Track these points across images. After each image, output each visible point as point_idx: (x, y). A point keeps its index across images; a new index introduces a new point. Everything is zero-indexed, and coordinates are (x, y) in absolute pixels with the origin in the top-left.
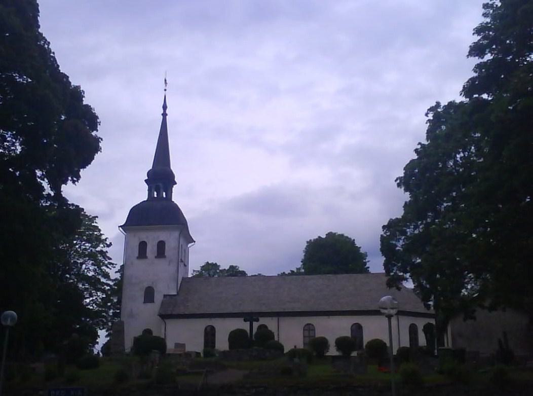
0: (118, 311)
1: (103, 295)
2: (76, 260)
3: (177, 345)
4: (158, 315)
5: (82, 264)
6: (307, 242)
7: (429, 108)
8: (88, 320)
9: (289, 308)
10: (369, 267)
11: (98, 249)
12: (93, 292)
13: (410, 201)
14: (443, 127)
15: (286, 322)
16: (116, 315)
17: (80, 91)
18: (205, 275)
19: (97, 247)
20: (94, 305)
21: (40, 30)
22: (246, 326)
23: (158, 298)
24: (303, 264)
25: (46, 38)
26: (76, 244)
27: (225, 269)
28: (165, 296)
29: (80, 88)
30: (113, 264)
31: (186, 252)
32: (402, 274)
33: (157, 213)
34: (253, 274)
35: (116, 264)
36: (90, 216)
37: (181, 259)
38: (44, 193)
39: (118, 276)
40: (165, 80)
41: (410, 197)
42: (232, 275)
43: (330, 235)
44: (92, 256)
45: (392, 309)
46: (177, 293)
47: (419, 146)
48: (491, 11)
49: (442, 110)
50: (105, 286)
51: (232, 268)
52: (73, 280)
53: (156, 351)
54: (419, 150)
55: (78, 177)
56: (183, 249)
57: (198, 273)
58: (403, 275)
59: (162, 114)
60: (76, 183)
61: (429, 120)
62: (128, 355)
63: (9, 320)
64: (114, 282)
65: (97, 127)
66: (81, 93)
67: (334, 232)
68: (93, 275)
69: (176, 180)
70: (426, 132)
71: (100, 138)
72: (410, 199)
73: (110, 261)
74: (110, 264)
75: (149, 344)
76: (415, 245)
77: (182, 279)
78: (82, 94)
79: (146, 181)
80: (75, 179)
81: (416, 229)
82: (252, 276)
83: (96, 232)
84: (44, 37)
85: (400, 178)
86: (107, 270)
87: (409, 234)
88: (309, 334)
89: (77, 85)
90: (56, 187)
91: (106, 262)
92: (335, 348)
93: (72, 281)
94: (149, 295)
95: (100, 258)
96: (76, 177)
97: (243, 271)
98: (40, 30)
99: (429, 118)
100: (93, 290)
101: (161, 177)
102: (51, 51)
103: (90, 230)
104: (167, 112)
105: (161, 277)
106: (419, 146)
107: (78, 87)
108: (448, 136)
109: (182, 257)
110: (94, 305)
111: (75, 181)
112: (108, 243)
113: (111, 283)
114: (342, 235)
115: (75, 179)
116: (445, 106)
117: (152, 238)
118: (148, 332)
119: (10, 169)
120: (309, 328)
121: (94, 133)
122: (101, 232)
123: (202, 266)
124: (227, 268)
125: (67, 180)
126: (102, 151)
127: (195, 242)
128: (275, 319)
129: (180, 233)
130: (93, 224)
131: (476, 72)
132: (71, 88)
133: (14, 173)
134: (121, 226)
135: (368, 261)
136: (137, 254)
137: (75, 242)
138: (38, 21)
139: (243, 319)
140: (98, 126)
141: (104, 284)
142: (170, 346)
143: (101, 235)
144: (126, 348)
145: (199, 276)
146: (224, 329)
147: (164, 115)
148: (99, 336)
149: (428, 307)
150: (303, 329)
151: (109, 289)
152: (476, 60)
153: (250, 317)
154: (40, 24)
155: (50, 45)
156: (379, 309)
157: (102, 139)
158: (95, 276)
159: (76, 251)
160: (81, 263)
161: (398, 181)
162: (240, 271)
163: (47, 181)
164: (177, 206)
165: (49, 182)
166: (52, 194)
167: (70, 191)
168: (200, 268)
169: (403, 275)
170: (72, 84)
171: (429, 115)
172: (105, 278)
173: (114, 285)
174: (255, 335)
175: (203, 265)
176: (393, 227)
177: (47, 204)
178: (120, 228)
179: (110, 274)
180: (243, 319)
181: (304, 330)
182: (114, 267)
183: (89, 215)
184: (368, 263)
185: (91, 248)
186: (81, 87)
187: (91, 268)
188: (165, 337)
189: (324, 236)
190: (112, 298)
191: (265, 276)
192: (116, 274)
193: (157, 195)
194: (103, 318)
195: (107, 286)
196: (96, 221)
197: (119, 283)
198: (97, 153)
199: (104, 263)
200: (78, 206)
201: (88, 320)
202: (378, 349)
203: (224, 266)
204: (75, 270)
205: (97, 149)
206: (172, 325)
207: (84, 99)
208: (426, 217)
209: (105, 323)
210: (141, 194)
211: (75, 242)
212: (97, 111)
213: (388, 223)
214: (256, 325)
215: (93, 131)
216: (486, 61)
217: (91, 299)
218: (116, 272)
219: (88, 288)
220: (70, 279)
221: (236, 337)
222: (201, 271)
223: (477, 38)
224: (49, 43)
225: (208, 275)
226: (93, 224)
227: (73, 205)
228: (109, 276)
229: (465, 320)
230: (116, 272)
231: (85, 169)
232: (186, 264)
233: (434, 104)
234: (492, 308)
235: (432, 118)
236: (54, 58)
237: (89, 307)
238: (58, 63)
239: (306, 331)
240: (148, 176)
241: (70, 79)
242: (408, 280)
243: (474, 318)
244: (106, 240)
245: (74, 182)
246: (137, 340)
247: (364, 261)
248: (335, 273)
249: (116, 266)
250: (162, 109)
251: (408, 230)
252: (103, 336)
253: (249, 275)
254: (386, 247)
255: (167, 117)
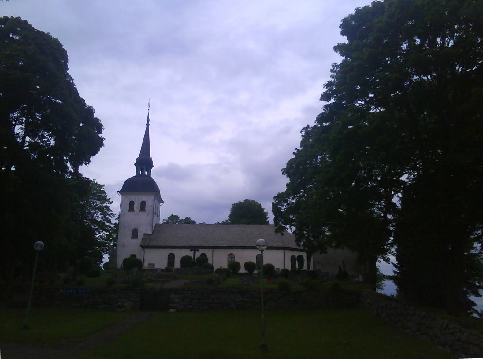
0: (116, 243)
1: (106, 233)
2: (90, 211)
3: (150, 264)
4: (140, 246)
5: (94, 213)
6: (233, 205)
7: (303, 128)
8: (97, 248)
9: (220, 243)
10: (268, 221)
11: (104, 205)
12: (100, 231)
13: (290, 183)
14: (311, 140)
15: (218, 252)
16: (115, 245)
17: (92, 109)
18: (170, 222)
19: (104, 203)
20: (101, 239)
21: (68, 72)
22: (191, 254)
23: (140, 235)
24: (230, 218)
25: (71, 76)
26: (91, 201)
27: (183, 219)
28: (145, 234)
29: (92, 107)
30: (113, 214)
31: (158, 208)
32: (284, 225)
33: (142, 184)
34: (200, 223)
35: (115, 214)
36: (100, 184)
37: (155, 213)
38: (68, 170)
39: (117, 221)
40: (149, 104)
41: (290, 181)
42: (186, 223)
43: (246, 201)
44: (101, 209)
45: (263, 246)
46: (152, 233)
47: (296, 151)
48: (335, 74)
49: (310, 130)
50: (108, 228)
51: (187, 218)
52: (88, 223)
53: (136, 267)
54: (296, 153)
55: (89, 161)
56: (157, 206)
57: (166, 221)
58: (285, 226)
59: (146, 124)
60: (88, 165)
61: (302, 136)
62: (119, 269)
63: (39, 246)
64: (114, 225)
65: (102, 131)
66: (93, 110)
67: (249, 199)
68: (101, 221)
69: (153, 164)
70: (300, 142)
71: (103, 138)
72: (290, 182)
73: (112, 212)
74: (112, 214)
75: (133, 263)
76: (292, 209)
77: (155, 225)
78: (94, 111)
79: (135, 164)
80: (87, 162)
81: (293, 199)
82: (199, 224)
83: (103, 194)
84: (70, 76)
85: (284, 169)
86: (110, 218)
87: (289, 202)
88: (231, 260)
89: (91, 105)
90: (76, 168)
91: (109, 213)
92: (244, 268)
93: (87, 224)
94: (135, 234)
95: (105, 210)
96: (88, 161)
97: (194, 221)
98: (68, 72)
99: (302, 134)
100: (100, 230)
101: (144, 162)
102: (74, 84)
103: (100, 193)
104: (149, 123)
105: (143, 223)
106: (296, 151)
107: (91, 107)
108: (312, 146)
109: (155, 211)
110: (101, 239)
111: (87, 164)
112: (111, 202)
113: (112, 226)
114: (254, 201)
115: (87, 162)
116: (312, 127)
117: (138, 199)
118: (134, 256)
119: (48, 155)
120: (231, 256)
121: (100, 135)
122: (106, 195)
123: (168, 217)
124: (184, 219)
125: (83, 163)
126: (105, 146)
127: (164, 202)
128: (211, 250)
129: (155, 196)
130: (101, 189)
131: (324, 110)
132: (86, 107)
133: (50, 157)
134: (119, 191)
135: (269, 217)
136: (128, 208)
137: (90, 200)
138: (67, 66)
139: (190, 249)
140: (103, 131)
141: (107, 226)
142: (146, 265)
143: (107, 196)
144: (118, 265)
145: (167, 223)
146: (179, 254)
147: (148, 125)
148: (104, 258)
149: (299, 245)
150: (227, 257)
151: (110, 229)
152: (325, 103)
153: (194, 249)
154: (68, 67)
155: (74, 81)
156: (255, 246)
157: (105, 139)
158: (102, 221)
159: (91, 205)
160: (93, 213)
161: (283, 171)
162: (192, 221)
163: (69, 163)
164: (154, 180)
165: (70, 164)
166: (73, 171)
167: (85, 171)
168: (167, 218)
169: (285, 226)
170: (87, 105)
171: (302, 132)
172: (108, 223)
173: (114, 227)
174: (197, 259)
175: (170, 216)
176: (280, 198)
177: (69, 177)
178: (118, 193)
179: (111, 221)
180: (190, 249)
181: (228, 257)
182: (114, 216)
183: (99, 184)
184: (268, 218)
185: (100, 204)
186: (93, 107)
187: (99, 216)
188: (213, 263)
189: (243, 201)
190: (112, 235)
191: (207, 224)
192: (116, 220)
193: (142, 173)
194: (106, 247)
195: (109, 227)
196: (104, 188)
197: (117, 226)
198: (102, 147)
199: (108, 213)
200: (89, 179)
201: (97, 248)
202: (270, 268)
203: (182, 217)
204: (90, 217)
205: (102, 145)
206: (148, 252)
207: (94, 114)
208: (299, 192)
209: (108, 250)
210: (132, 172)
211: (90, 200)
212: (102, 122)
213: (277, 195)
214: (198, 254)
215: (99, 134)
216: (330, 103)
217: (99, 235)
218: (116, 219)
219: (97, 228)
220: (86, 222)
221: (185, 261)
222: (168, 220)
223: (325, 90)
224: (73, 79)
225: (172, 223)
226: (101, 189)
227: (85, 178)
228: (111, 221)
229: (320, 254)
230: (116, 219)
231: (94, 157)
232: (158, 215)
233: (306, 126)
234: (336, 247)
235: (304, 134)
236: (76, 89)
237: (97, 240)
238: (78, 92)
239: (229, 258)
240: (136, 161)
241: (86, 102)
242: (288, 229)
243: (326, 253)
244: (109, 199)
245: (86, 164)
246: (125, 261)
247: (266, 217)
248: (249, 223)
249: (115, 216)
250: (146, 121)
251: (289, 200)
252: (106, 258)
253: (197, 223)
254: (276, 210)
255: (149, 126)
